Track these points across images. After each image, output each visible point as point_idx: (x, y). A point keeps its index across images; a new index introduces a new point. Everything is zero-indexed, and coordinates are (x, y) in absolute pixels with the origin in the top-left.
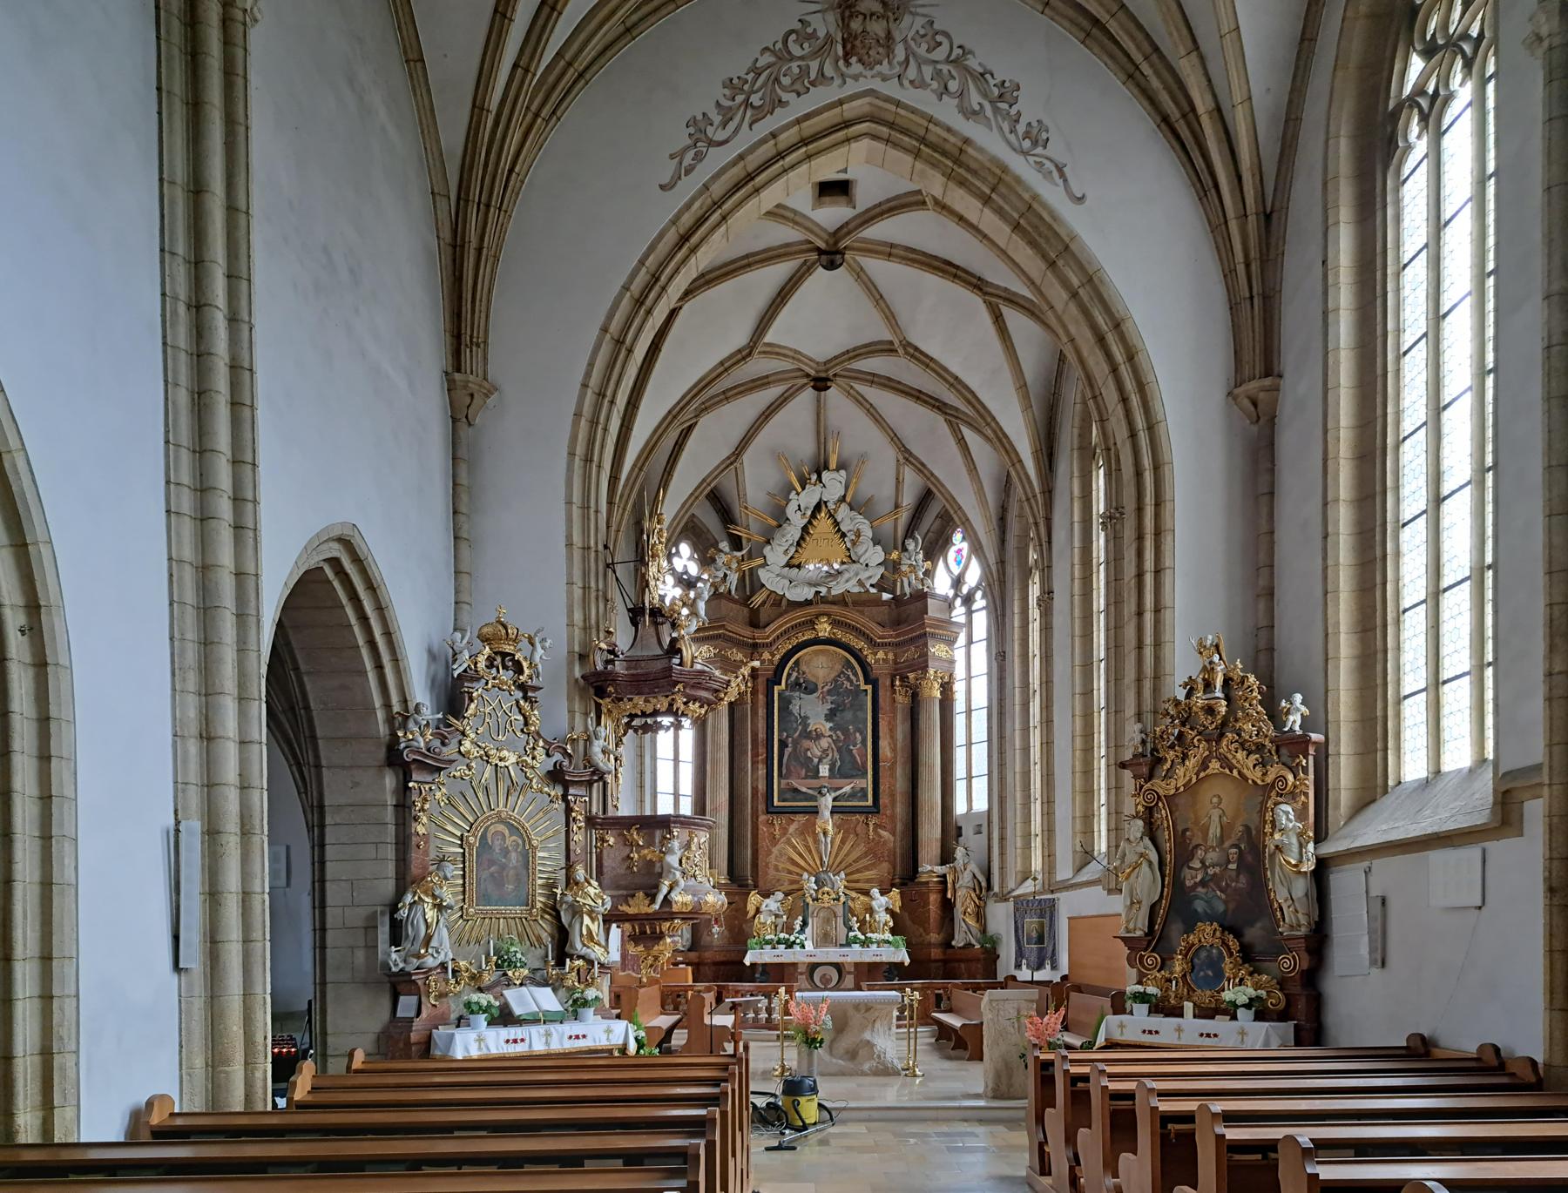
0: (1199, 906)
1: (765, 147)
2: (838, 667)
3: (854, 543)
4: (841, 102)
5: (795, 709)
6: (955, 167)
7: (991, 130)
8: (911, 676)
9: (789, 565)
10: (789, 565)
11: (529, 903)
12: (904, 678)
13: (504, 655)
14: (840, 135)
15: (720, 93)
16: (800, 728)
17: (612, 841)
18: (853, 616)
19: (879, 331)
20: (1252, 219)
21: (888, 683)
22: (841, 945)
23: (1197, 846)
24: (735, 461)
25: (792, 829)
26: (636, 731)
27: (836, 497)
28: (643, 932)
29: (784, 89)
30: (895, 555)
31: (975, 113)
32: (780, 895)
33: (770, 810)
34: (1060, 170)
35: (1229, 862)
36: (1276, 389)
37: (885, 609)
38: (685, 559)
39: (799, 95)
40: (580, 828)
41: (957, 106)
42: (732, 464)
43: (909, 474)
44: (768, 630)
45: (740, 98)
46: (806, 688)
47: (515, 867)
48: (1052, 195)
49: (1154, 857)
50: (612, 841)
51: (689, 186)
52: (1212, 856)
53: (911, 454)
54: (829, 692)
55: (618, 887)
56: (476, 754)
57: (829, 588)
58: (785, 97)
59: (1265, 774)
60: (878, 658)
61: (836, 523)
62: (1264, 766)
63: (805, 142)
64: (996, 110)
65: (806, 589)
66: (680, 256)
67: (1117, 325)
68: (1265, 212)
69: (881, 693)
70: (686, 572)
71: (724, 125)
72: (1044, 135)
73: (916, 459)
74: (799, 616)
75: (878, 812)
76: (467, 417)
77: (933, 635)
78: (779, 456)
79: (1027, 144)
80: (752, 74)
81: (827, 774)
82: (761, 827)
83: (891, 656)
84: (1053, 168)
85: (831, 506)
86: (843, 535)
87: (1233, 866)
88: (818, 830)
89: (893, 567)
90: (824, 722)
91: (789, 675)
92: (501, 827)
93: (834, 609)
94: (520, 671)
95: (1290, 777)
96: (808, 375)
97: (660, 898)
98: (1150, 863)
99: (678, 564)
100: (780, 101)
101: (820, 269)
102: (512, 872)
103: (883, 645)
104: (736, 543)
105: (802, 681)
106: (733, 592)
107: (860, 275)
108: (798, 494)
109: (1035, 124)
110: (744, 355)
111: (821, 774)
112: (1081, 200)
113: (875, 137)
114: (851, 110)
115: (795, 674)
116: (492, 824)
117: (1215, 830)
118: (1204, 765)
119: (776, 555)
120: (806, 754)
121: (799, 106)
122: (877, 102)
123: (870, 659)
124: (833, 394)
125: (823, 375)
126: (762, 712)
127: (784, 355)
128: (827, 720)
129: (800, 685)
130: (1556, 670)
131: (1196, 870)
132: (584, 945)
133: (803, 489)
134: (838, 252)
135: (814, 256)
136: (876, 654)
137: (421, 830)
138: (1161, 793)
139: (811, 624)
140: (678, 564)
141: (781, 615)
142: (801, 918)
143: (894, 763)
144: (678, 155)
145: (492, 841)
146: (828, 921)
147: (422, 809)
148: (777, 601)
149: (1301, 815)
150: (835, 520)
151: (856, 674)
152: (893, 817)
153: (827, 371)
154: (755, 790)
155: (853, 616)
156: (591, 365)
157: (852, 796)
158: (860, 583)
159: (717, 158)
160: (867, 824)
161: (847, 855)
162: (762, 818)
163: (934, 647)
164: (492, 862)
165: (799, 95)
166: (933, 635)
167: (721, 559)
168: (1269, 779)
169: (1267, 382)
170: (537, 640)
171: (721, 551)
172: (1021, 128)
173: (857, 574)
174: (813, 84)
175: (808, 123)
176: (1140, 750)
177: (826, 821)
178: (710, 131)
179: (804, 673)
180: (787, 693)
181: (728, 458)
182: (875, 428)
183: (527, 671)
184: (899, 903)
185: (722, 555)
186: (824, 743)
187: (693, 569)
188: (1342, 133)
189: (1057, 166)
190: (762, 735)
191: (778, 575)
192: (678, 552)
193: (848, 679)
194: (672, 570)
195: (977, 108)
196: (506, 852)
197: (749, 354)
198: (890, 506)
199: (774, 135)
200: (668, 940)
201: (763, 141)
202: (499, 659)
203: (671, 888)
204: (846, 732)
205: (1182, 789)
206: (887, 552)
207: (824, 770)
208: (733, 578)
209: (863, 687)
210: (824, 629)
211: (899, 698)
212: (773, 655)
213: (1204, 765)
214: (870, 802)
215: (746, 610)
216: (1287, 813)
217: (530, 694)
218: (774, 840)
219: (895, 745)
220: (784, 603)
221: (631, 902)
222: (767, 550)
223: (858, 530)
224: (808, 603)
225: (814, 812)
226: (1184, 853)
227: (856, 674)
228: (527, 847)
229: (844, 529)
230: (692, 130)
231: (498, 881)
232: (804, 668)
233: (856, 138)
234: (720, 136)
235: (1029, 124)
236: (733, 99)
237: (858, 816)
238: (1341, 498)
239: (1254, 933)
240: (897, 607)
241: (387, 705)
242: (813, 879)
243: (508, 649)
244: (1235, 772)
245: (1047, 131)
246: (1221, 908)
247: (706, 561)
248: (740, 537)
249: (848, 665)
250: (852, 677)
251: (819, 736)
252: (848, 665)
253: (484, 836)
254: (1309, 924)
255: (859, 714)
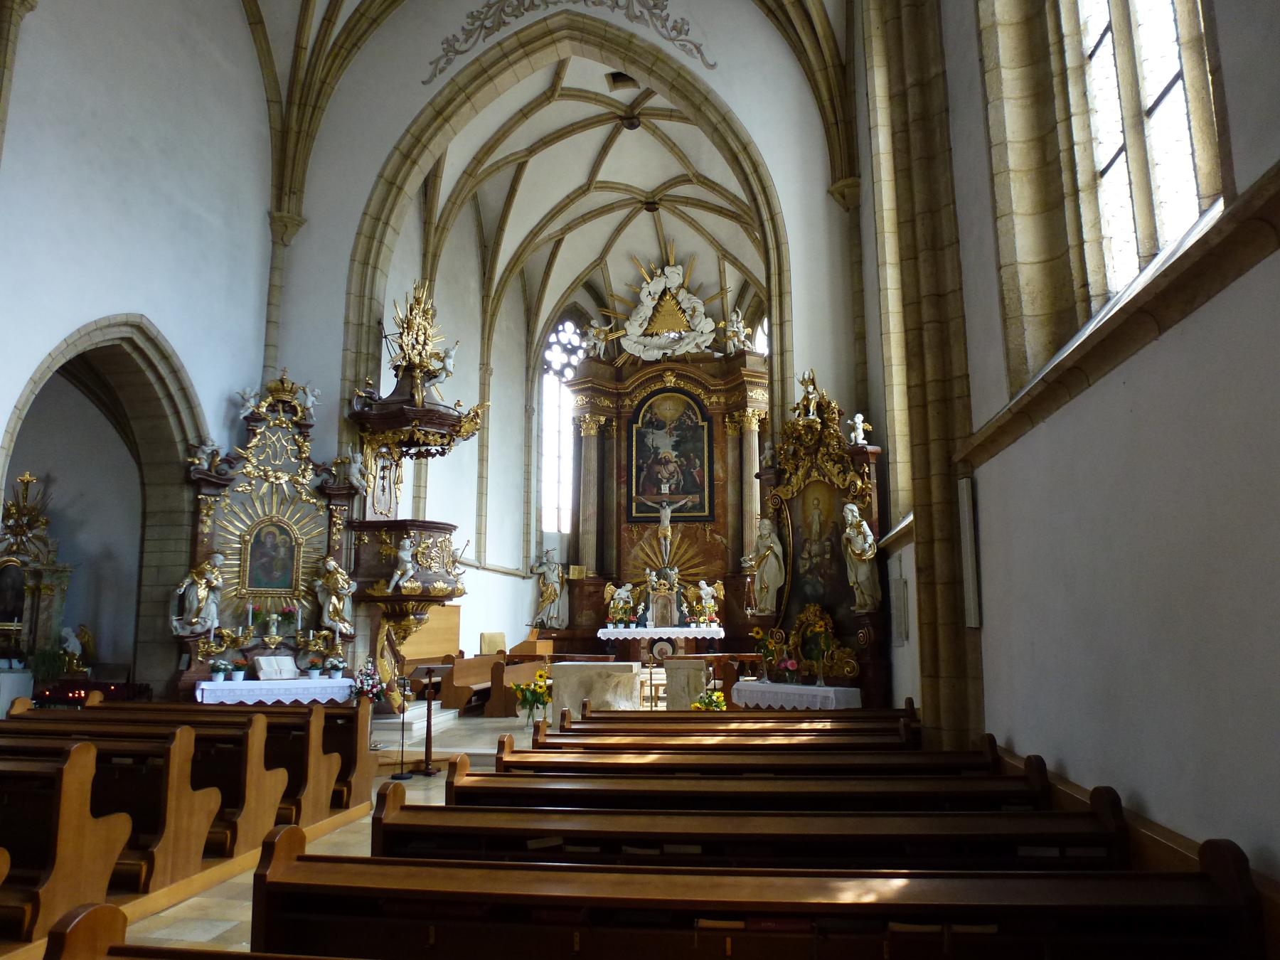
0: (808, 589)
1: (493, 51)
2: (681, 409)
3: (692, 316)
4: (545, 19)
5: (649, 441)
6: (627, 52)
7: (649, 27)
8: (736, 414)
9: (645, 335)
10: (645, 335)
11: (291, 585)
12: (731, 417)
13: (284, 402)
14: (547, 39)
15: (465, 22)
16: (653, 456)
17: (366, 539)
18: (691, 370)
19: (676, 169)
20: (831, 70)
21: (720, 420)
22: (675, 626)
23: (805, 541)
24: (600, 263)
25: (646, 534)
26: (411, 458)
27: (677, 284)
28: (394, 610)
29: (507, 15)
30: (722, 324)
31: (637, 17)
32: (629, 586)
33: (631, 520)
34: (698, 48)
35: (825, 553)
36: (858, 185)
37: (716, 364)
38: (569, 332)
39: (517, 17)
40: (339, 530)
41: (625, 14)
42: (598, 265)
43: (729, 268)
44: (627, 383)
45: (478, 23)
46: (657, 426)
47: (283, 559)
48: (693, 65)
49: (778, 549)
50: (366, 539)
51: (441, 81)
52: (815, 548)
53: (726, 252)
54: (675, 428)
55: (369, 575)
56: (256, 474)
57: (674, 351)
58: (507, 19)
59: (845, 480)
60: (713, 401)
61: (678, 303)
62: (844, 474)
63: (522, 45)
64: (652, 15)
65: (656, 352)
66: (435, 125)
67: (745, 148)
68: (841, 64)
69: (715, 428)
70: (570, 343)
71: (466, 41)
72: (686, 27)
73: (731, 255)
74: (650, 372)
75: (713, 521)
76: (282, 239)
77: (751, 383)
78: (632, 258)
79: (674, 34)
80: (486, 9)
81: (667, 492)
82: (623, 533)
83: (722, 400)
84: (692, 47)
85: (674, 291)
86: (684, 311)
87: (828, 556)
88: (660, 535)
89: (720, 334)
90: (671, 451)
91: (644, 416)
92: (273, 529)
93: (678, 366)
94: (295, 413)
95: (859, 483)
96: (641, 202)
97: (393, 584)
98: (777, 557)
99: (564, 338)
100: (504, 22)
101: (625, 129)
102: (279, 563)
103: (715, 392)
104: (607, 320)
105: (654, 420)
106: (602, 356)
107: (655, 131)
108: (648, 283)
109: (679, 21)
110: (583, 191)
111: (663, 492)
112: (713, 66)
113: (572, 38)
114: (552, 23)
115: (649, 415)
116: (265, 526)
117: (816, 527)
118: (808, 475)
119: (634, 328)
120: (657, 476)
121: (516, 25)
122: (570, 17)
123: (706, 402)
124: (663, 212)
125: (651, 200)
126: (624, 444)
127: (620, 189)
128: (673, 450)
129: (653, 423)
130: (913, 384)
131: (806, 559)
132: (332, 620)
133: (652, 279)
134: (634, 117)
135: (619, 122)
136: (710, 398)
137: (206, 530)
138: (783, 498)
139: (660, 377)
140: (564, 338)
141: (638, 371)
142: (643, 604)
143: (726, 482)
144: (437, 61)
145: (265, 538)
146: (665, 606)
147: (207, 515)
148: (635, 361)
149: (865, 513)
150: (677, 301)
151: (695, 414)
152: (725, 525)
153: (654, 197)
154: (619, 504)
155: (691, 370)
156: (370, 199)
157: (693, 508)
158: (697, 346)
159: (461, 62)
160: (705, 530)
161: (682, 556)
162: (624, 526)
163: (751, 392)
164: (263, 555)
165: (517, 17)
166: (751, 383)
167: (592, 332)
168: (847, 483)
169: (850, 181)
170: (307, 390)
171: (593, 327)
172: (670, 24)
173: (695, 339)
174: (527, 10)
175: (523, 34)
176: (770, 463)
177: (666, 528)
178: (457, 45)
179: (656, 414)
180: (643, 430)
181: (595, 261)
182: (698, 236)
183: (300, 414)
184: (722, 593)
185: (593, 330)
186: (671, 467)
187: (576, 341)
188: (871, 7)
189: (695, 46)
190: (624, 462)
191: (635, 342)
192: (564, 330)
193: (689, 417)
194: (558, 342)
195: (639, 14)
196: (275, 547)
197: (588, 189)
198: (716, 290)
199: (499, 44)
200: (412, 617)
201: (492, 48)
202: (280, 406)
203: (402, 575)
204: (688, 459)
205: (795, 494)
206: (717, 323)
207: (665, 489)
208: (602, 346)
209: (701, 423)
210: (670, 380)
211: (730, 432)
212: (632, 401)
213: (808, 475)
214: (707, 513)
215: (612, 369)
216: (852, 511)
217: (303, 430)
218: (633, 544)
219: (727, 469)
220: (640, 362)
221: (375, 587)
222: (627, 324)
223: (694, 307)
224: (657, 362)
225: (658, 521)
226: (800, 546)
227: (695, 414)
228: (294, 544)
229: (683, 307)
230: (445, 46)
231: (268, 569)
232: (656, 410)
233: (559, 40)
234: (464, 47)
235: (676, 21)
236: (473, 24)
237: (697, 524)
238: (888, 262)
239: (842, 612)
240: (726, 362)
241: (185, 439)
242: (654, 573)
243: (287, 398)
244: (827, 480)
245: (688, 24)
246: (821, 590)
247: (583, 335)
248: (610, 316)
249: (689, 407)
250: (692, 416)
251: (667, 462)
252: (689, 407)
253: (258, 536)
254: (873, 604)
255: (698, 444)
